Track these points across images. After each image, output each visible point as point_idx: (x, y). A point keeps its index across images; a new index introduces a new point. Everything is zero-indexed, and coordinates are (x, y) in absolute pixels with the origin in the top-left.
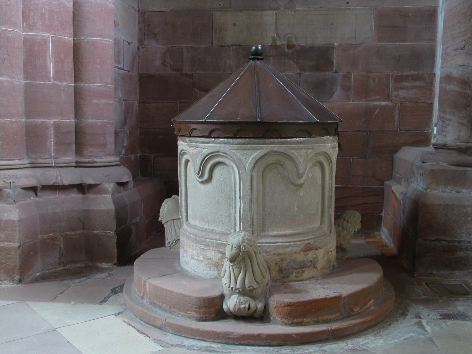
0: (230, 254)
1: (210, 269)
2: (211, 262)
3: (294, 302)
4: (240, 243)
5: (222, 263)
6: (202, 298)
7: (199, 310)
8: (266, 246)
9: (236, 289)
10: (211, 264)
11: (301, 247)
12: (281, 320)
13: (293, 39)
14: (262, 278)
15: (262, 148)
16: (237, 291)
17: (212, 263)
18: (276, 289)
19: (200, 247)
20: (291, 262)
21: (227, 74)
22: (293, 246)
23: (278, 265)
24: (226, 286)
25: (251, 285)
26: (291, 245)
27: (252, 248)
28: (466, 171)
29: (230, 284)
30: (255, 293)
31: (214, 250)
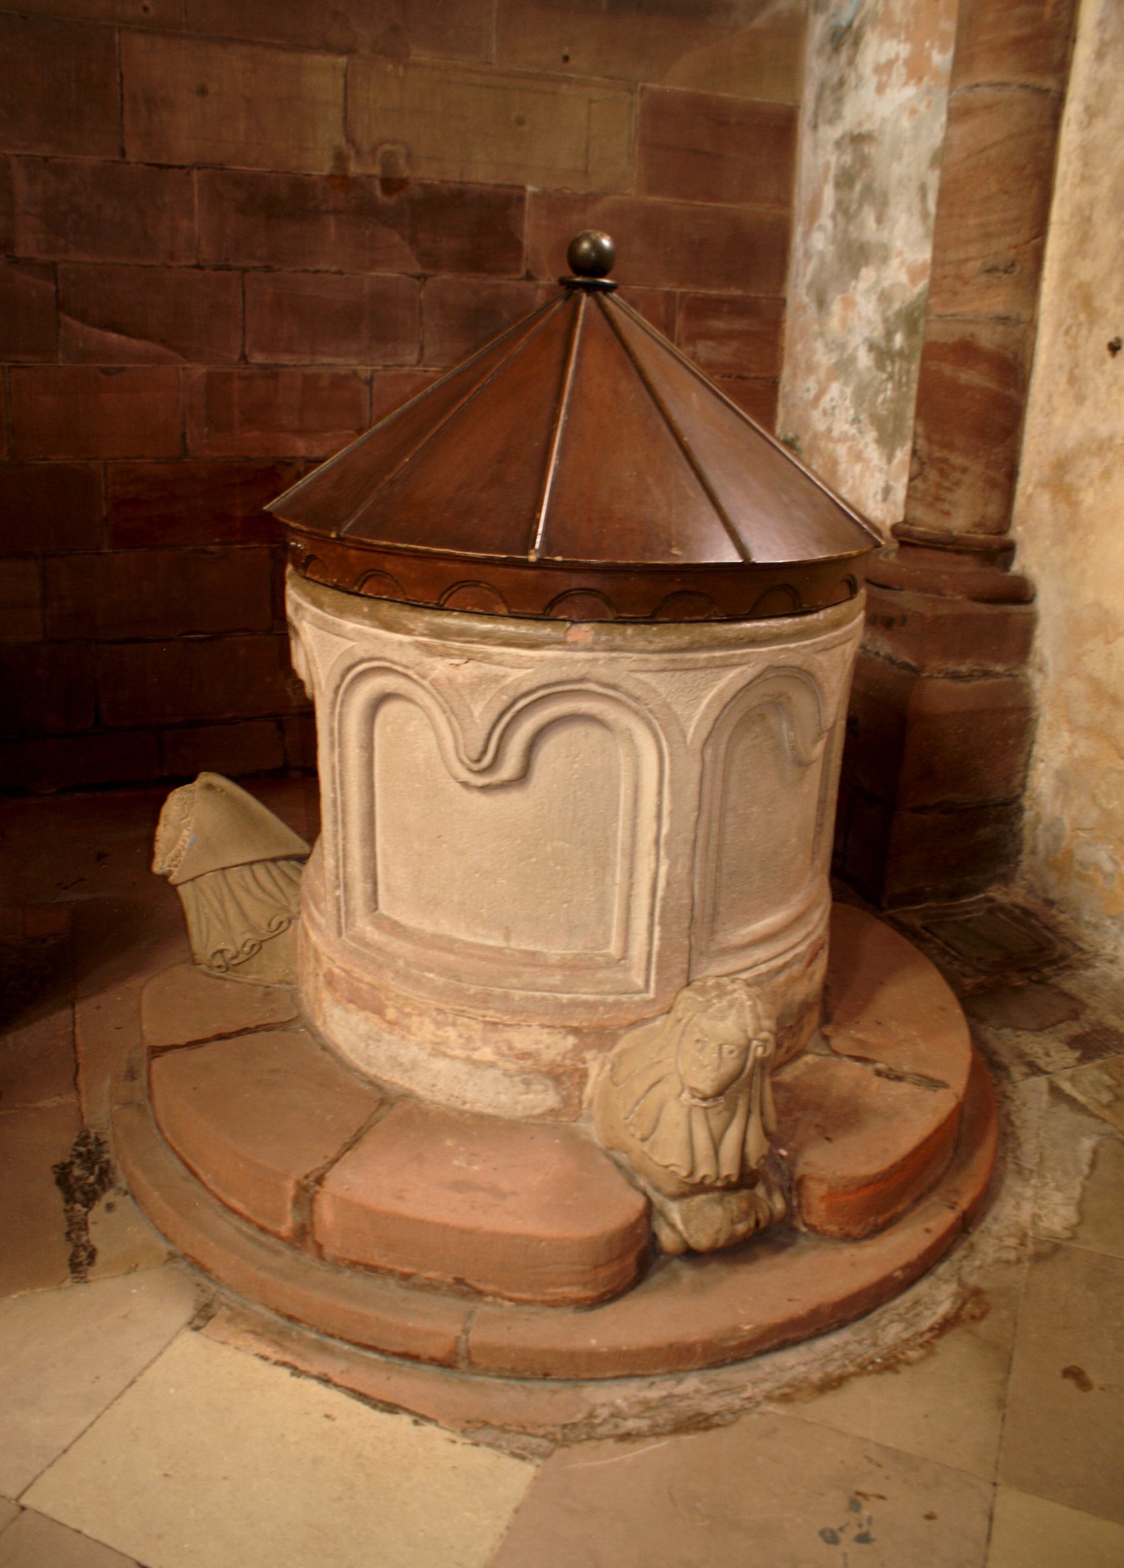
2: (534, 1065)
5: (581, 1066)
13: (402, 162)
15: (744, 661)
19: (481, 1019)
21: (180, 267)
28: (1009, 615)
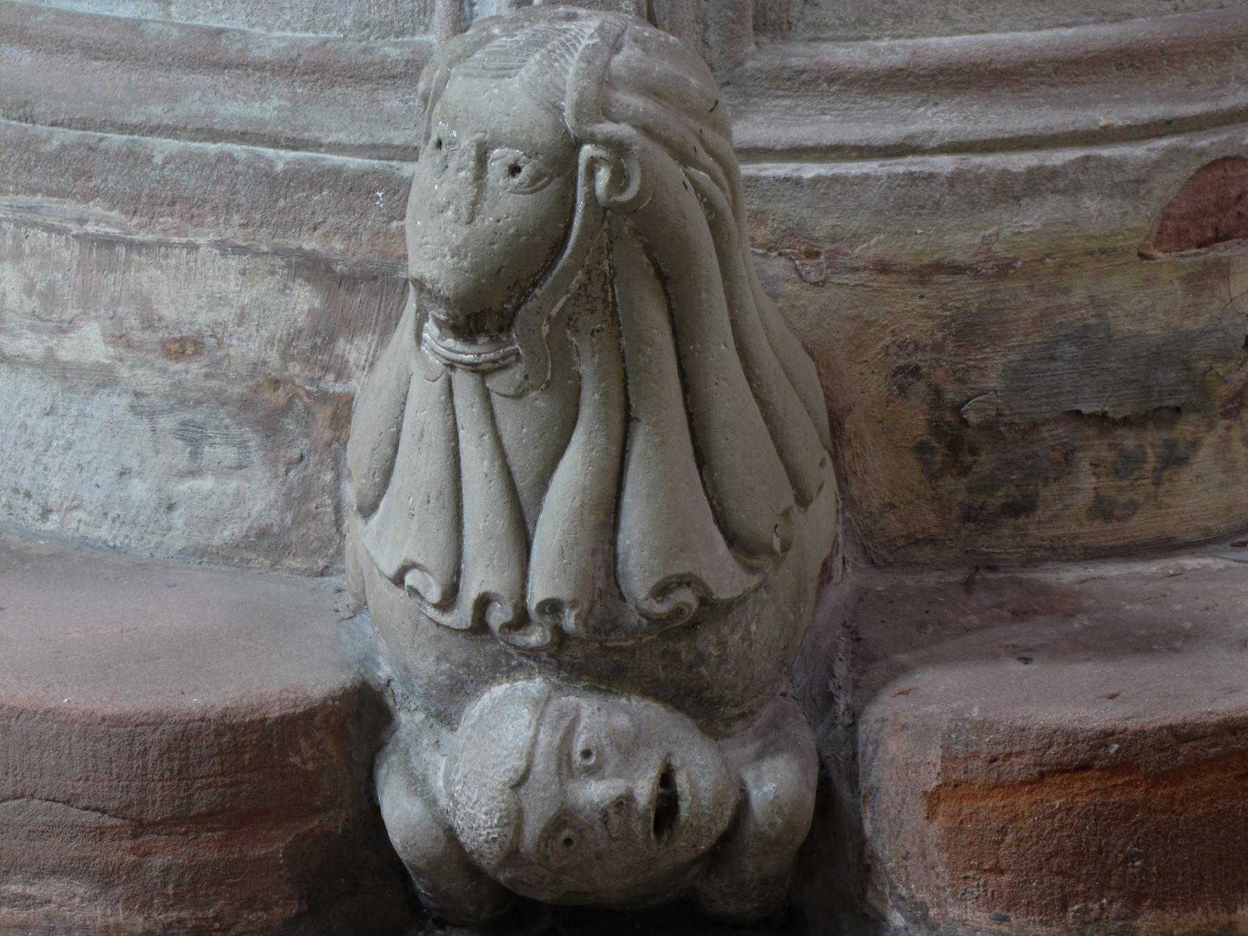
0: (456, 239)
1: (195, 455)
2: (207, 376)
3: (1141, 733)
4: (569, 122)
5: (330, 384)
6: (157, 722)
7: (131, 858)
8: (798, 182)
9: (521, 620)
10: (199, 403)
11: (1158, 192)
12: (1003, 919)
14: (789, 499)
16: (536, 637)
17: (213, 383)
18: (922, 626)
19: (75, 229)
20: (1052, 358)
22: (1078, 188)
23: (921, 387)
24: (413, 591)
25: (684, 567)
26: (1054, 173)
27: (692, 170)
29: (458, 572)
30: (723, 659)
31: (240, 250)
